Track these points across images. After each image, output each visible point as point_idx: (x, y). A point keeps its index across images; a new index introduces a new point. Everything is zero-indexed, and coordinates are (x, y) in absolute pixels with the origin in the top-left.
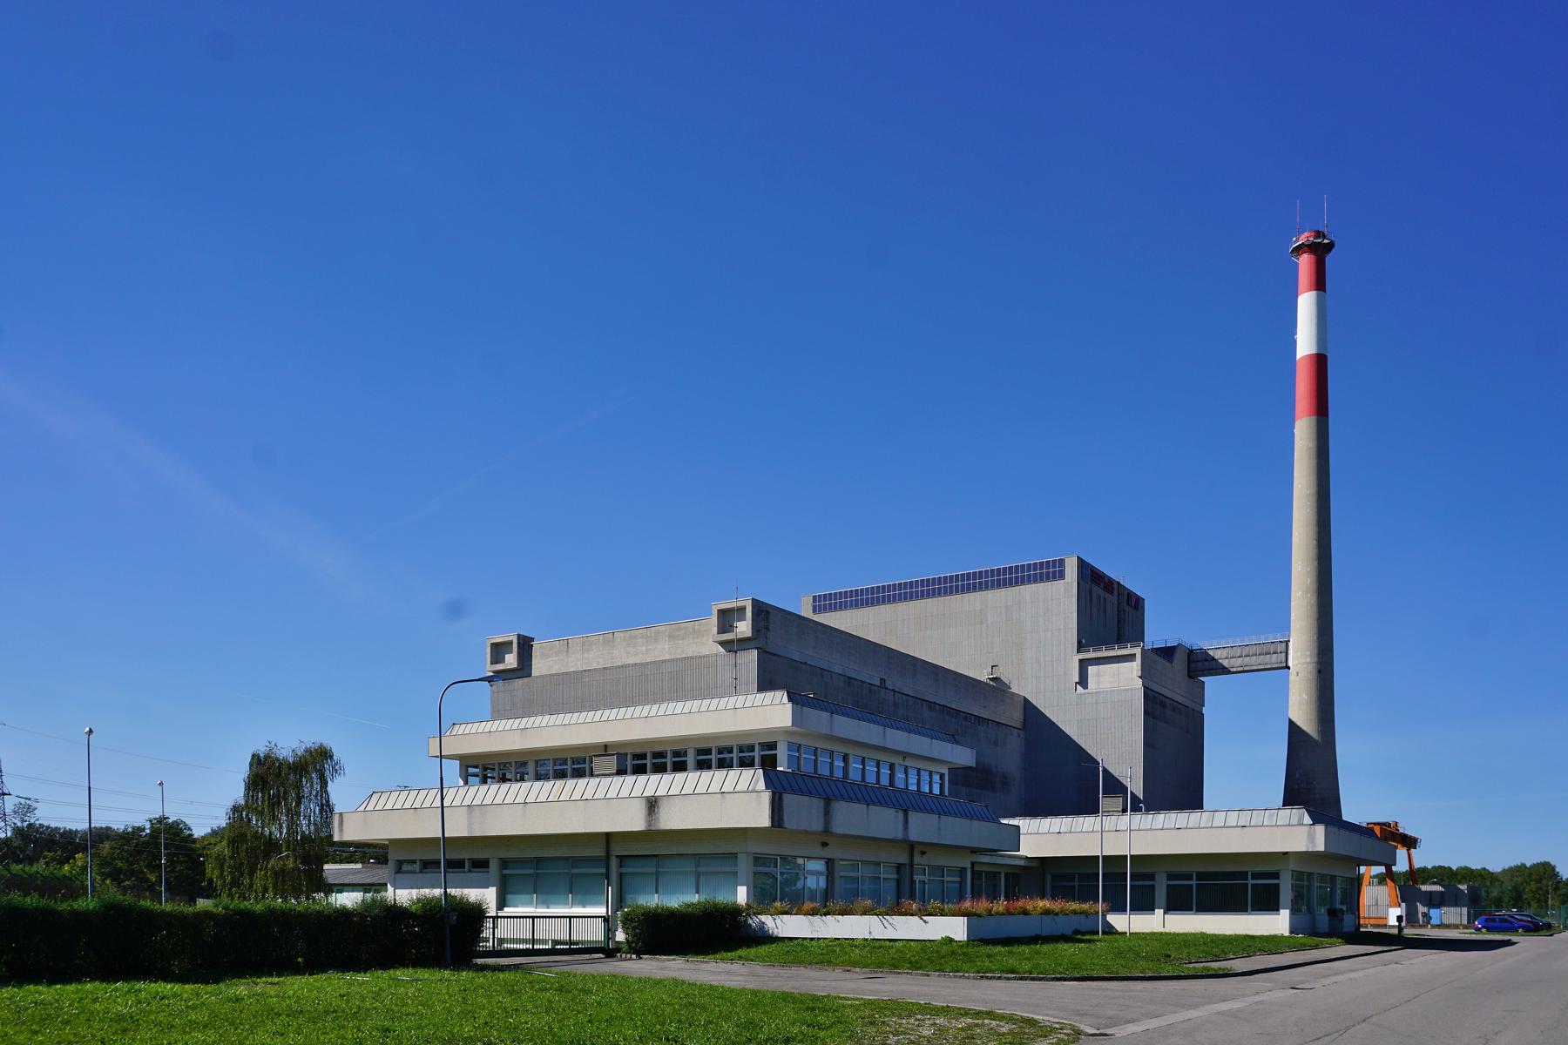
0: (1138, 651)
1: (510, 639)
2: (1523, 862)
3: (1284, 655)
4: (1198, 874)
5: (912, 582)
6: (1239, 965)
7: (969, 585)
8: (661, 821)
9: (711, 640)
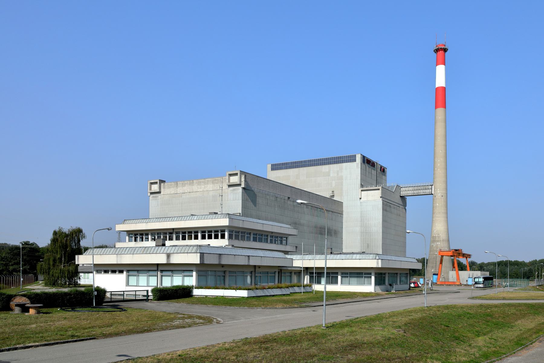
0: (380, 188)
2: (536, 259)
3: (431, 190)
4: (350, 273)
8: (171, 261)
9: (226, 184)
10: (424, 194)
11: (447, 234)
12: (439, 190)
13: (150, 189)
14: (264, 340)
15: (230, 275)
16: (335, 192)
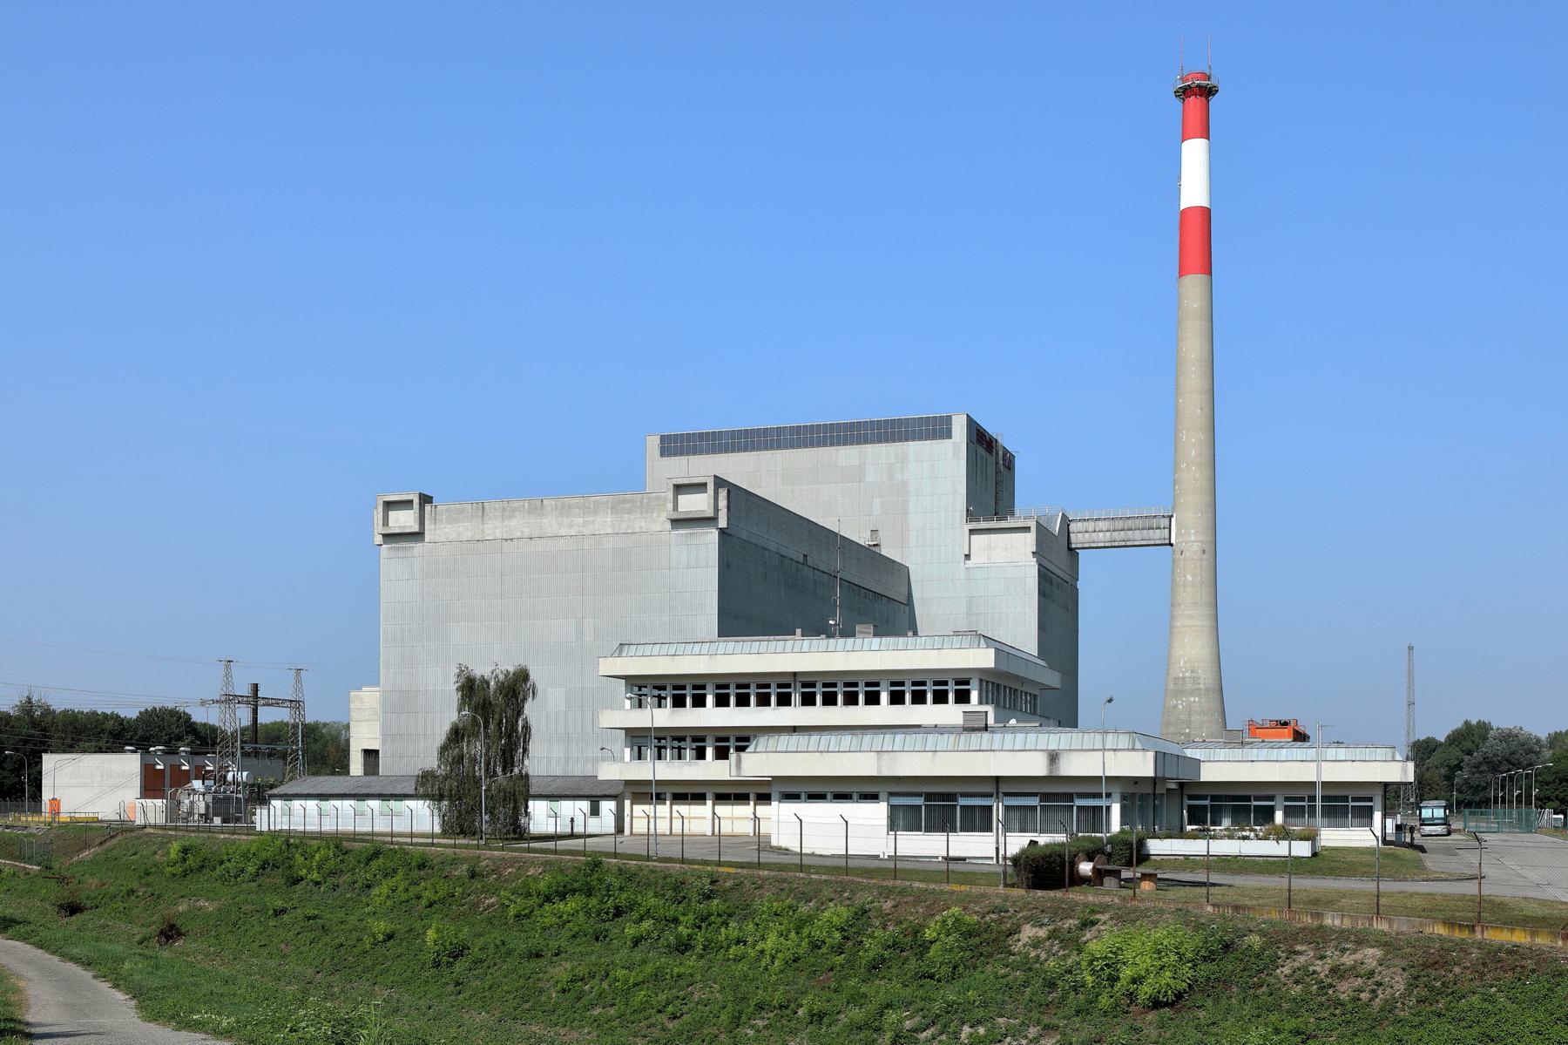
1: (410, 498)
3: (1167, 531)
10: (1145, 543)
12: (1188, 532)
13: (386, 523)
16: (880, 534)
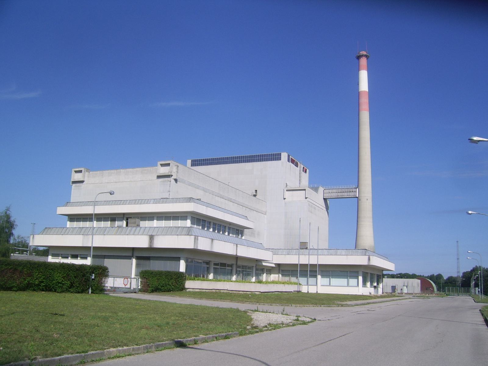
5: (252, 155)
6: (349, 303)
7: (225, 161)
11: (359, 220)
14: (72, 352)
15: (351, 275)
